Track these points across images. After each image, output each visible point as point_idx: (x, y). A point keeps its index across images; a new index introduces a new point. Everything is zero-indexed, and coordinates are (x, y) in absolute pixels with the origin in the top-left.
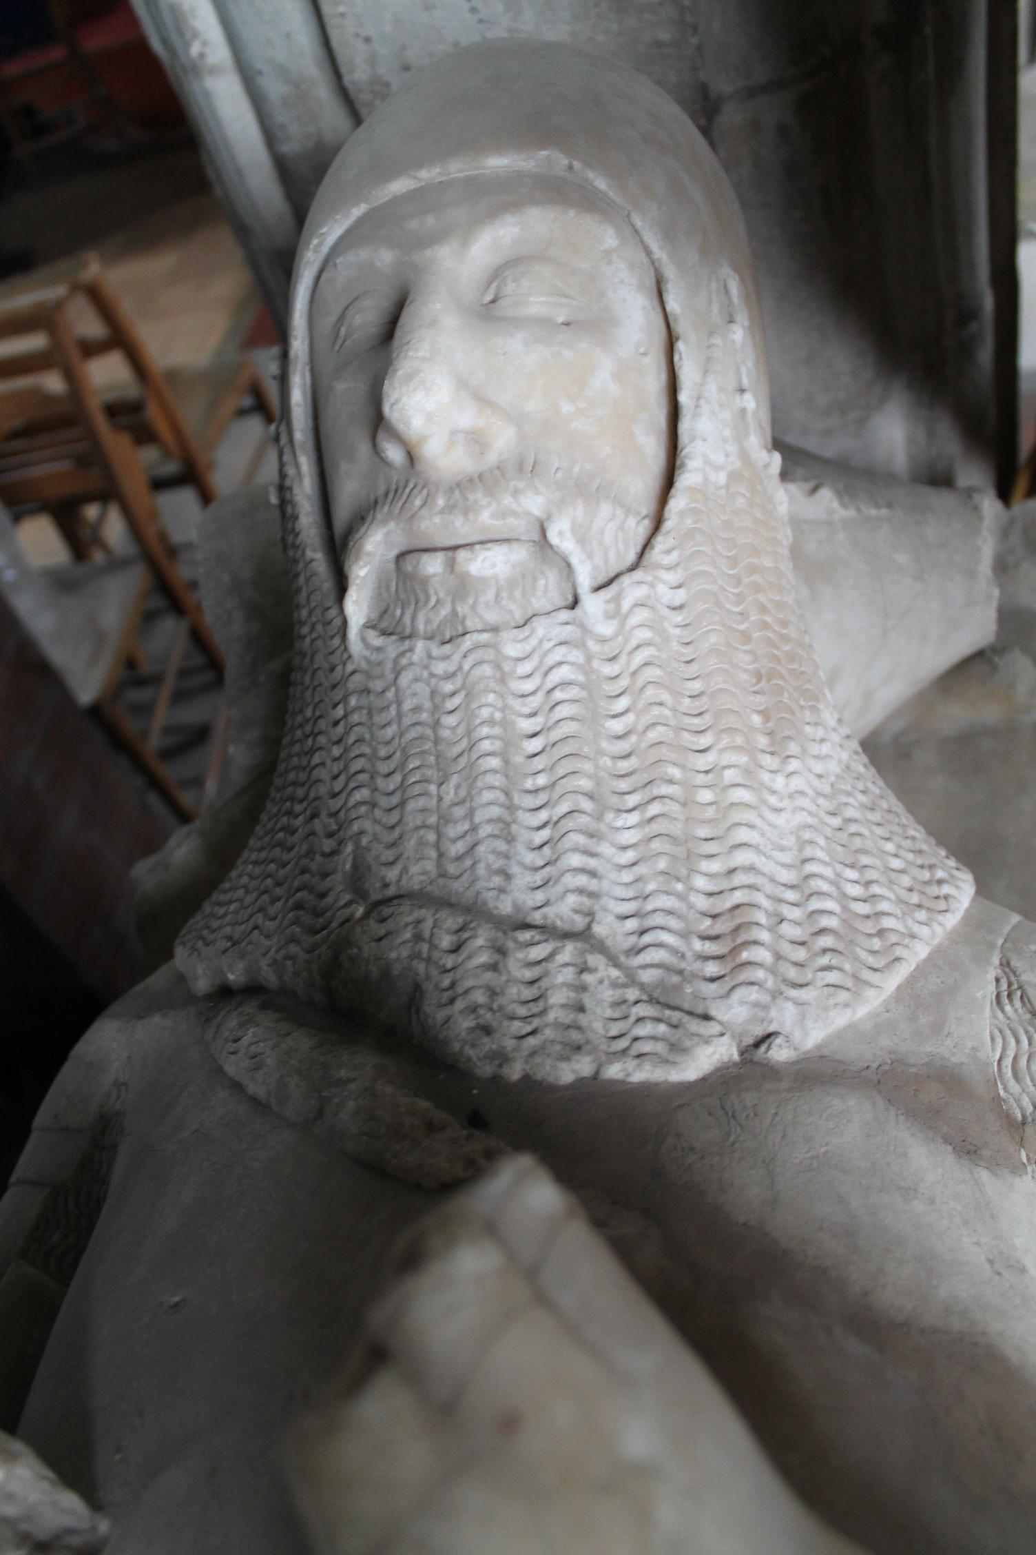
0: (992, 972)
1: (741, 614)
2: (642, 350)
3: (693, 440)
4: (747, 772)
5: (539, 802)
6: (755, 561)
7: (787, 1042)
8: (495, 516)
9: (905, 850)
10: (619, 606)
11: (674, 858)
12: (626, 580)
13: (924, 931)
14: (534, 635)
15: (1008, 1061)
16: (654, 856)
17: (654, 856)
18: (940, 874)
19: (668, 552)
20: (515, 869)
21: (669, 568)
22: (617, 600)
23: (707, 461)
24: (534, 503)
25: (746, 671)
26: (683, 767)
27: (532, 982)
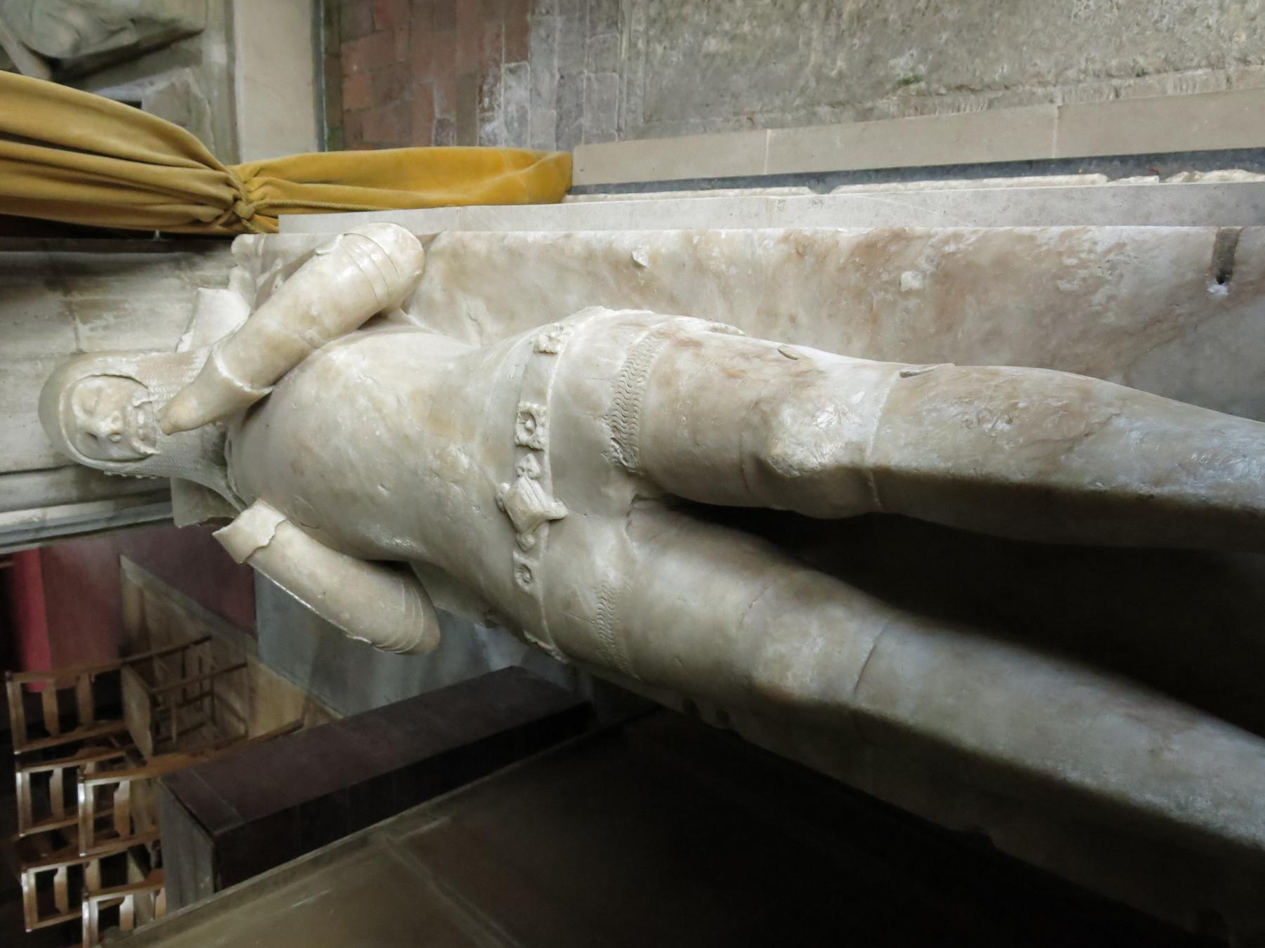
22: (152, 394)
24: (130, 408)
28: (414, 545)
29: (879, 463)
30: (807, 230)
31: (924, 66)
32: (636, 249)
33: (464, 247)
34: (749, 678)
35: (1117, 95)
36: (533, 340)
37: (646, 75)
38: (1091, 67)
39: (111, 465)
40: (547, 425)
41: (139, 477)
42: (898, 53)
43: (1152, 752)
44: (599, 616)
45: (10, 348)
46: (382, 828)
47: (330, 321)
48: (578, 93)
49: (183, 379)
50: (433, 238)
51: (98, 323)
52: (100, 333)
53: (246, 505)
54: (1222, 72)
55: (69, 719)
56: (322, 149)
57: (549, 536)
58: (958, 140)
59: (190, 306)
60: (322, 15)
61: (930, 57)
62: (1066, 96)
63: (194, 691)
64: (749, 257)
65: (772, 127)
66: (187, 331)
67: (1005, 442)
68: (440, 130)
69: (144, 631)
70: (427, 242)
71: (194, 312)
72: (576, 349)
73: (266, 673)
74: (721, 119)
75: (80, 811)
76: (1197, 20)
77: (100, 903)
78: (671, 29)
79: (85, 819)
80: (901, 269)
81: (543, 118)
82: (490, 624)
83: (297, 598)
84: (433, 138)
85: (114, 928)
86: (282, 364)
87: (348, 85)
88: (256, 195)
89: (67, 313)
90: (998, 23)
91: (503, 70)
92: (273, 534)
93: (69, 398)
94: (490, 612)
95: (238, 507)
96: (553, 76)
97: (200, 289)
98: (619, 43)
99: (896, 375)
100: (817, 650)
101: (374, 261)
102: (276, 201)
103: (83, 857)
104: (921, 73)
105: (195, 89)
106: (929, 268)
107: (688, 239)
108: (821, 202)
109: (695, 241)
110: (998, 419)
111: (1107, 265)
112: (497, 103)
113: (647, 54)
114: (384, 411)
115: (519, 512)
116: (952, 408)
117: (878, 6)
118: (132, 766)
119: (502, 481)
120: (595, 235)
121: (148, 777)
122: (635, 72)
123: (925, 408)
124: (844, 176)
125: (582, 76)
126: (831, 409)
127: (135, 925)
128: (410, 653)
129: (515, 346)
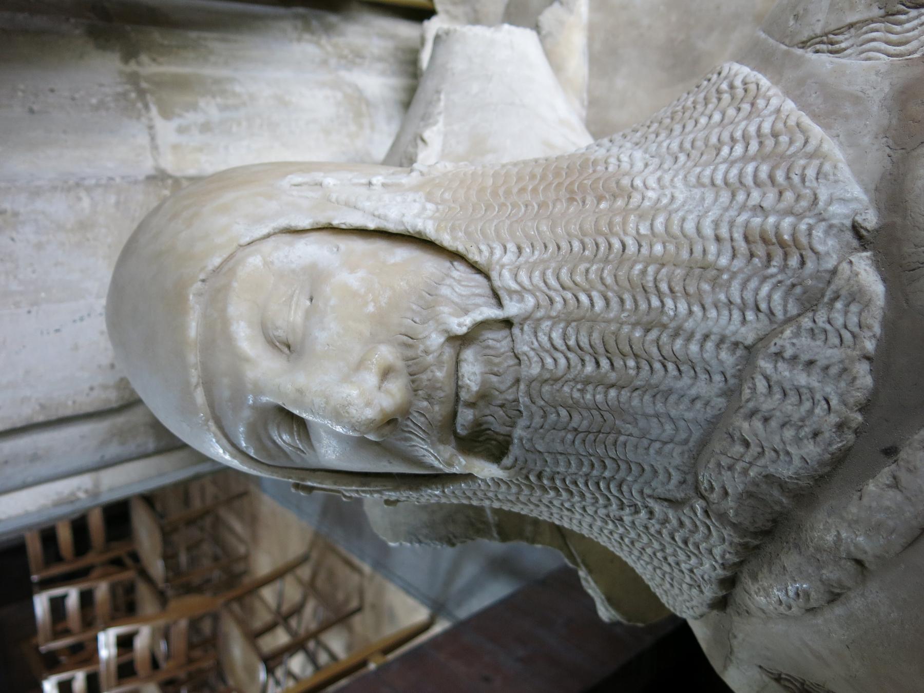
0: (809, 55)
1: (526, 206)
2: (335, 250)
3: (403, 223)
4: (641, 217)
5: (647, 368)
6: (489, 191)
7: (861, 214)
8: (440, 369)
9: (705, 109)
10: (516, 292)
11: (700, 278)
12: (497, 283)
13: (774, 102)
14: (527, 353)
15: (891, 49)
16: (699, 292)
17: (699, 292)
18: (724, 86)
19: (480, 251)
20: (693, 392)
21: (492, 253)
22: (511, 292)
23: (418, 215)
25: (568, 208)
26: (635, 263)
27: (785, 394)
51: (191, 117)
89: (133, 95)
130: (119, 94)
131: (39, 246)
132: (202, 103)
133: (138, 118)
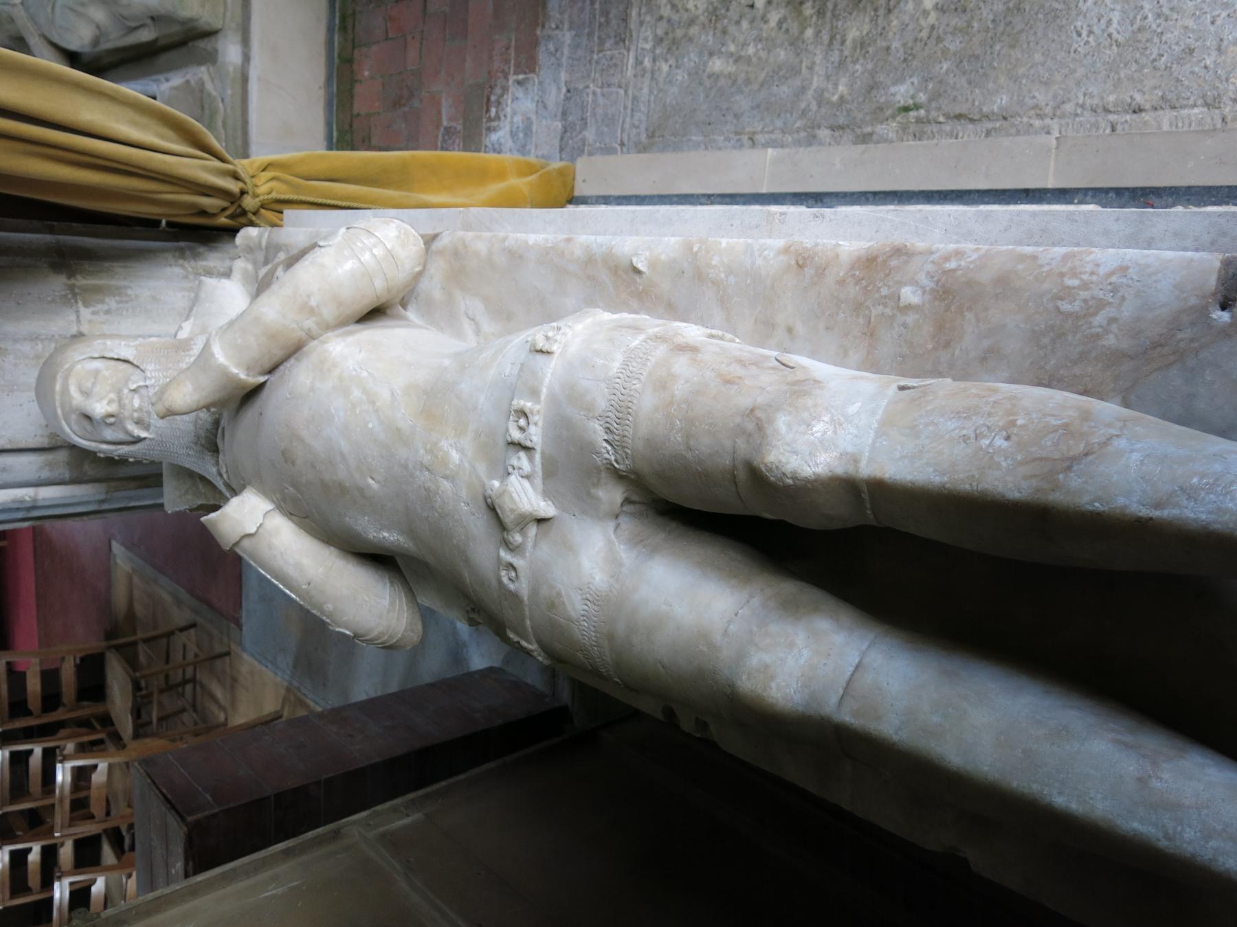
24: (126, 391)
28: (401, 539)
29: (873, 475)
30: (808, 243)
31: (924, 94)
32: (636, 254)
33: (465, 246)
34: (732, 686)
35: (1113, 130)
36: (530, 339)
37: (651, 92)
38: (1088, 102)
39: (104, 447)
40: (540, 424)
41: (131, 460)
42: (900, 80)
43: (1140, 780)
44: (582, 618)
45: (11, 328)
46: (354, 822)
47: (329, 313)
48: (583, 108)
49: (181, 365)
50: (435, 237)
51: (100, 307)
52: (102, 317)
53: (235, 492)
54: (1217, 111)
55: (51, 699)
56: (330, 148)
57: (536, 535)
58: (956, 167)
59: (192, 295)
60: (337, 21)
61: (931, 86)
62: (1063, 129)
63: (177, 677)
64: (749, 266)
65: (774, 147)
66: (187, 318)
67: (1003, 459)
68: (446, 137)
69: (131, 616)
70: (430, 240)
71: (195, 302)
72: (572, 349)
73: (247, 663)
74: (722, 138)
75: (57, 791)
76: (1195, 60)
77: (71, 884)
78: (677, 48)
79: (61, 800)
80: (901, 284)
81: (547, 130)
82: (472, 623)
83: (281, 586)
84: (439, 144)
85: (82, 909)
86: (278, 353)
87: (358, 89)
88: (262, 189)
89: (70, 296)
90: (998, 55)
91: (511, 82)
92: (261, 522)
93: (66, 378)
94: (473, 610)
95: (228, 495)
96: (559, 89)
97: (202, 278)
98: (625, 60)
99: (894, 387)
100: (802, 661)
101: (374, 256)
102: (282, 197)
103: (58, 837)
104: (920, 101)
105: (209, 86)
106: (928, 284)
107: (688, 246)
108: (823, 216)
109: (695, 249)
110: (996, 435)
111: (1109, 287)
112: (503, 113)
113: (653, 73)
114: (378, 404)
115: (508, 509)
116: (949, 423)
117: (881, 34)
118: (111, 748)
119: (493, 478)
120: (596, 240)
121: (127, 760)
122: (641, 89)
123: (922, 421)
124: (842, 197)
125: (588, 90)
126: (826, 419)
127: (105, 907)
128: (390, 647)
129: (512, 344)
130: (62, 296)
131: (16, 365)
132: (107, 300)
133: (71, 307)
